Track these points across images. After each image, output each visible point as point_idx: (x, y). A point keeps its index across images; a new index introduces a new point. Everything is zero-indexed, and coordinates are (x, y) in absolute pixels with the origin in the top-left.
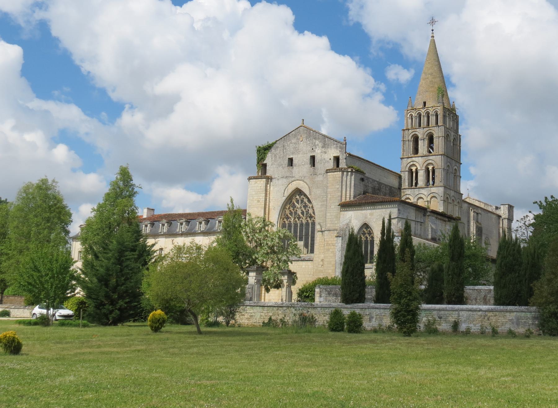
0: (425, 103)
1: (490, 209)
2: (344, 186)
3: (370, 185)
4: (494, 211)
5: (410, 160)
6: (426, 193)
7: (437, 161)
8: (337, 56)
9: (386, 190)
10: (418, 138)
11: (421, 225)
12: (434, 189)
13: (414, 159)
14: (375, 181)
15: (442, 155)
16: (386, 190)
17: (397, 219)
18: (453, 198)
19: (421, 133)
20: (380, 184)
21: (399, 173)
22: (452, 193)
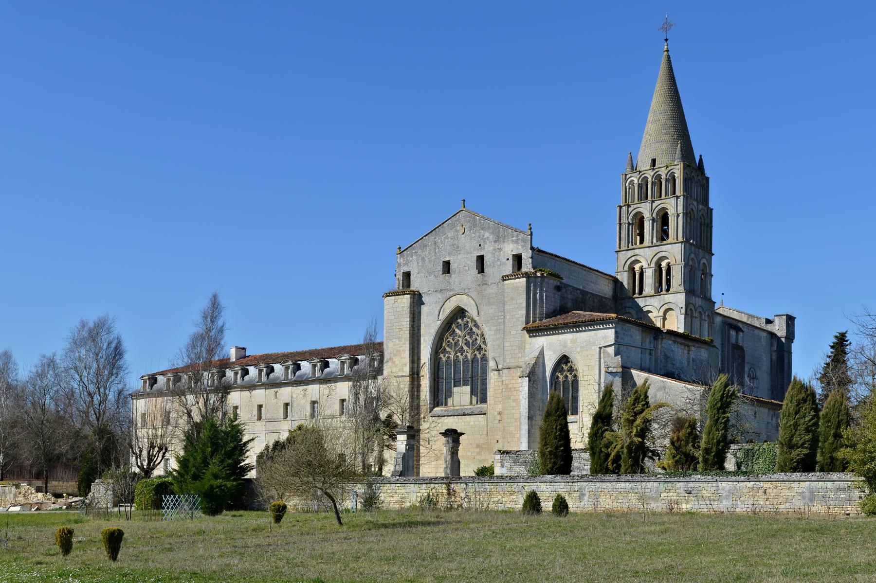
0: (654, 161)
3: (569, 296)
5: (630, 253)
6: (656, 304)
7: (674, 252)
9: (593, 301)
10: (643, 217)
11: (650, 354)
12: (668, 298)
13: (637, 252)
14: (577, 289)
16: (593, 301)
18: (700, 310)
19: (645, 209)
20: (584, 293)
22: (698, 301)
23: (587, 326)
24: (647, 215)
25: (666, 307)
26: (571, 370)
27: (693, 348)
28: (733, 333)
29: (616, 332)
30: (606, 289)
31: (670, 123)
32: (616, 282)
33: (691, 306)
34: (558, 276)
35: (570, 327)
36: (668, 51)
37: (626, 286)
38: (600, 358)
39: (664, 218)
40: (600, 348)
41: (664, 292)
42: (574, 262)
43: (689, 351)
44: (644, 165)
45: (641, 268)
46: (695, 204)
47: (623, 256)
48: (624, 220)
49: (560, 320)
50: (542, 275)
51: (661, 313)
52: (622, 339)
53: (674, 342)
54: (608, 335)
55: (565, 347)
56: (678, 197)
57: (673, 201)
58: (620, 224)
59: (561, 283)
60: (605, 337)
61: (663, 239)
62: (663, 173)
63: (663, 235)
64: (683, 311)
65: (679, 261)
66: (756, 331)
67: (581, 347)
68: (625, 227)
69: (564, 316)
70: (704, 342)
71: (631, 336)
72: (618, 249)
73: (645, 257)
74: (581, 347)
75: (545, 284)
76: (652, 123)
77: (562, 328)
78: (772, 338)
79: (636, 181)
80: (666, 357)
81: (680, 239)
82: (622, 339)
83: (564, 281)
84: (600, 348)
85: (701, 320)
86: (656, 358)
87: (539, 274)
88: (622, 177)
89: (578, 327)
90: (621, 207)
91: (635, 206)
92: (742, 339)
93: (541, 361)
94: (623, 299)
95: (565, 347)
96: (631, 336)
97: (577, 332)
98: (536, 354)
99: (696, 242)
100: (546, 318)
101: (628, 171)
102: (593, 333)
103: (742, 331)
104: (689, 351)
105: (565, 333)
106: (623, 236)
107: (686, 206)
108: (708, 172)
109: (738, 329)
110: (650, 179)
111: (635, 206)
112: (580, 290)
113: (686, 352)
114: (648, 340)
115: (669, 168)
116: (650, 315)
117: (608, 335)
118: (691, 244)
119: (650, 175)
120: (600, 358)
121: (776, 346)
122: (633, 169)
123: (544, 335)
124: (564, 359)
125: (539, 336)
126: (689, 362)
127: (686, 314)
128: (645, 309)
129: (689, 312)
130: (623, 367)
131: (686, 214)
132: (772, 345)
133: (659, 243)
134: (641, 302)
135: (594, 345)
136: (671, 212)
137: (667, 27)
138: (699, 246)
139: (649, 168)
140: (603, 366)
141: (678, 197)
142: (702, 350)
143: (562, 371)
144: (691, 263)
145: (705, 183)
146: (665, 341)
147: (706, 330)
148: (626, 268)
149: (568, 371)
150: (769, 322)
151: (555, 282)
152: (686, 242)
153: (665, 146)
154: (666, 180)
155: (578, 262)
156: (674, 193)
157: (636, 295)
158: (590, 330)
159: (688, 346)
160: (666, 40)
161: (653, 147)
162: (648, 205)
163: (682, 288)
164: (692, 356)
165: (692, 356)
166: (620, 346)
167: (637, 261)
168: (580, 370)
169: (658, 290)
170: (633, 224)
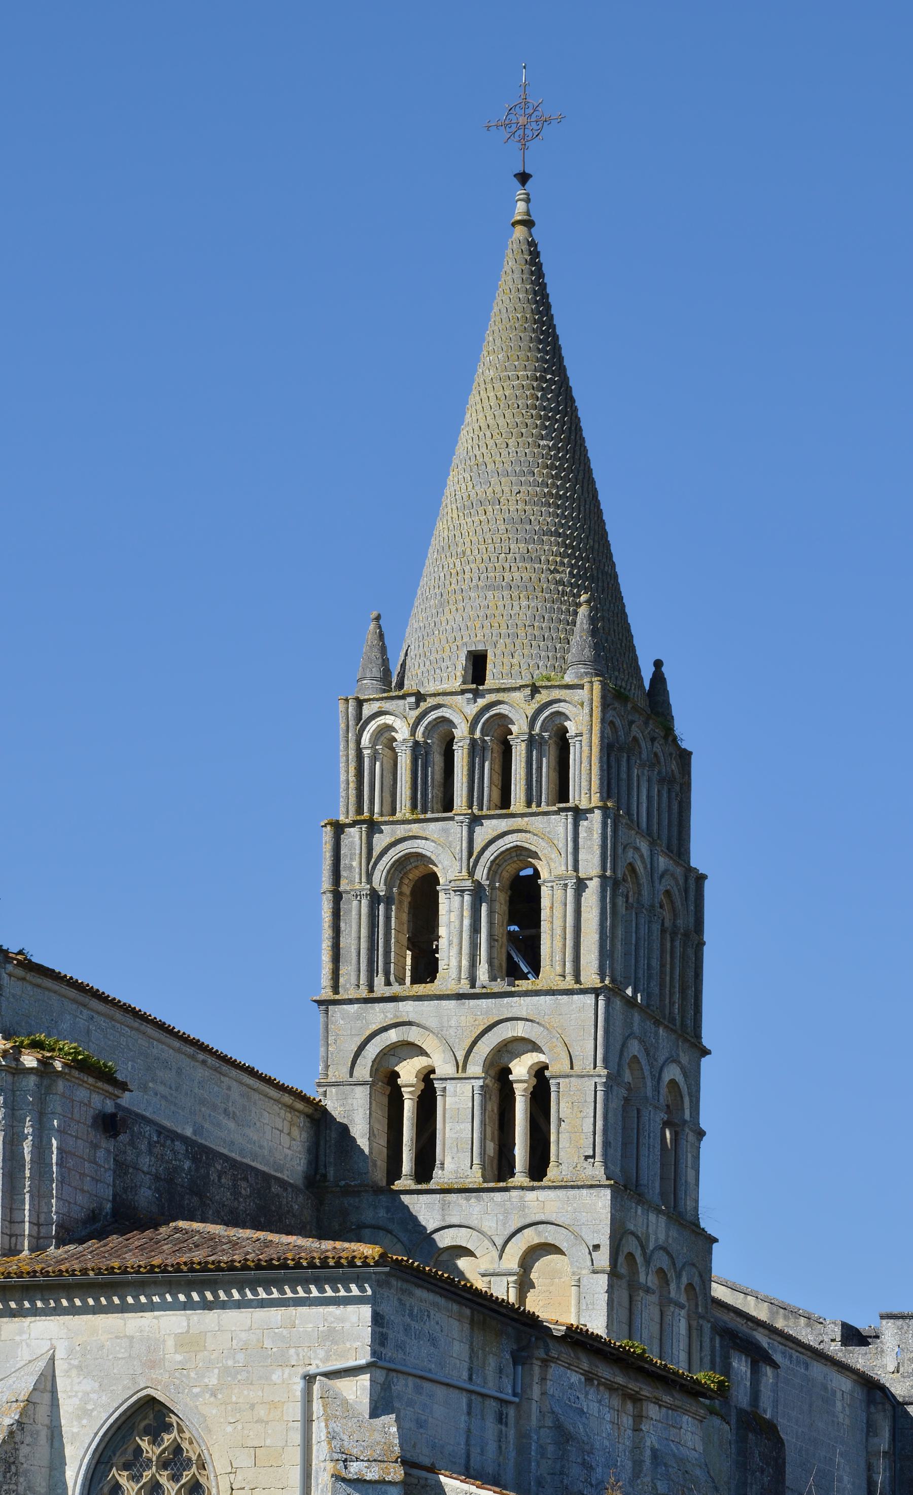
0: (477, 664)
1: (808, 1336)
2: (587, 1164)
3: (145, 1162)
4: (835, 1349)
5: (380, 1014)
6: (489, 1225)
7: (564, 1028)
8: (637, 648)
9: (236, 1194)
10: (432, 879)
11: (501, 1419)
12: (540, 1202)
13: (408, 1010)
14: (175, 1136)
15: (596, 992)
16: (236, 1194)
17: (365, 1380)
18: (661, 1261)
19: (444, 847)
20: (201, 1154)
21: (313, 1093)
22: (657, 1228)
23: (253, 1285)
24: (449, 869)
25: (530, 1237)
26: (176, 1460)
27: (652, 1410)
28: (741, 1366)
29: (377, 1319)
30: (281, 1148)
31: (544, 518)
32: (320, 1123)
33: (631, 1245)
34: (105, 1076)
35: (173, 1286)
36: (528, 223)
37: (363, 1143)
38: (308, 1420)
39: (518, 896)
40: (309, 1379)
41: (520, 1178)
42: (161, 1026)
43: (639, 1418)
44: (436, 670)
45: (427, 1077)
46: (644, 847)
47: (351, 1023)
48: (353, 880)
49: (128, 1252)
50: (45, 1063)
51: (511, 1261)
52: (400, 1347)
53: (589, 1378)
54: (346, 1327)
55: (153, 1365)
56: (579, 814)
57: (560, 825)
58: (337, 896)
59: (118, 1106)
60: (331, 1336)
61: (513, 973)
62: (519, 712)
63: (519, 954)
64: (603, 1259)
65: (584, 1062)
66: (818, 1370)
67: (226, 1371)
68: (356, 912)
69: (137, 1239)
70: (694, 1390)
71: (433, 1341)
72: (326, 993)
73: (446, 1033)
74: (226, 1371)
75: (55, 1104)
76: (469, 506)
77: (140, 1286)
78: (870, 1401)
79: (402, 732)
80: (563, 1436)
81: (590, 976)
82: (400, 1347)
83: (126, 1099)
84: (309, 1379)
85: (665, 1302)
86: (523, 1437)
87: (29, 1060)
88: (344, 712)
89: (213, 1285)
90: (338, 828)
91: (401, 831)
92: (777, 1396)
93: (42, 1414)
94: (347, 1192)
95: (153, 1365)
96: (433, 1341)
97: (207, 1306)
98: (25, 1385)
99: (648, 996)
100: (61, 1242)
101: (369, 688)
102: (276, 1315)
103: (775, 1365)
104: (639, 1418)
105: (151, 1307)
106: (348, 942)
107: (613, 850)
108: (687, 728)
109: (759, 1357)
110: (461, 731)
111: (401, 831)
112: (184, 1139)
113: (627, 1421)
114: (492, 1362)
115: (544, 697)
116: (463, 1263)
117: (346, 1327)
118: (630, 1003)
119: (461, 713)
120: (308, 1420)
121: (886, 1434)
122: (391, 682)
123: (59, 1311)
124: (147, 1416)
125: (35, 1312)
126: (637, 1464)
127: (613, 1274)
128: (444, 1240)
129: (623, 1269)
130: (407, 1463)
131: (612, 884)
132: (871, 1429)
133: (500, 986)
134: (426, 1210)
135: (282, 1362)
136: (551, 868)
137: (526, 123)
138: (654, 1013)
139: (456, 684)
140: (320, 1451)
141: (579, 814)
142: (686, 1420)
143: (135, 1463)
144: (627, 1076)
145: (674, 772)
146: (554, 1370)
147: (683, 1344)
148: (363, 1071)
149: (164, 1465)
150: (853, 1337)
151: (98, 1100)
152: (610, 992)
153: (523, 608)
154: (532, 742)
155: (180, 1026)
156: (562, 794)
157: (404, 1182)
158: (262, 1304)
159: (636, 1399)
160: (523, 178)
161: (468, 600)
162: (456, 831)
163: (597, 1171)
164: (651, 1441)
165: (651, 1441)
166: (391, 1375)
167: (413, 1049)
168: (218, 1463)
169: (500, 1168)
170: (389, 900)
